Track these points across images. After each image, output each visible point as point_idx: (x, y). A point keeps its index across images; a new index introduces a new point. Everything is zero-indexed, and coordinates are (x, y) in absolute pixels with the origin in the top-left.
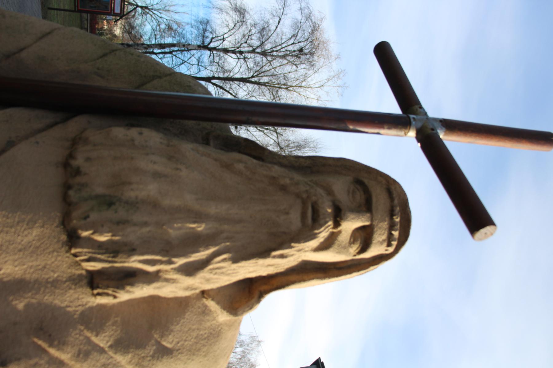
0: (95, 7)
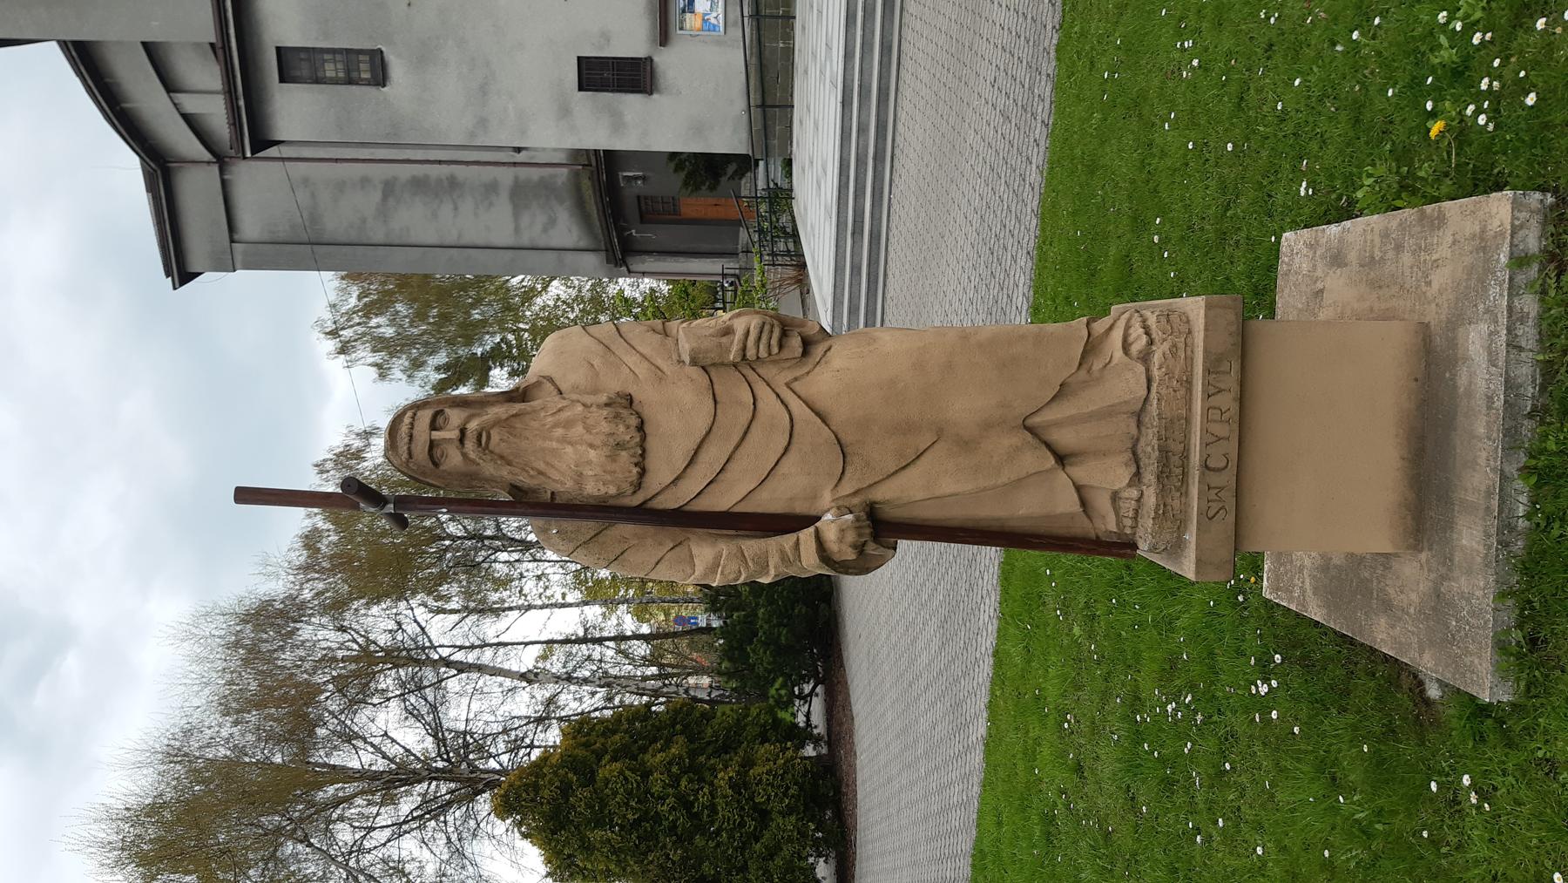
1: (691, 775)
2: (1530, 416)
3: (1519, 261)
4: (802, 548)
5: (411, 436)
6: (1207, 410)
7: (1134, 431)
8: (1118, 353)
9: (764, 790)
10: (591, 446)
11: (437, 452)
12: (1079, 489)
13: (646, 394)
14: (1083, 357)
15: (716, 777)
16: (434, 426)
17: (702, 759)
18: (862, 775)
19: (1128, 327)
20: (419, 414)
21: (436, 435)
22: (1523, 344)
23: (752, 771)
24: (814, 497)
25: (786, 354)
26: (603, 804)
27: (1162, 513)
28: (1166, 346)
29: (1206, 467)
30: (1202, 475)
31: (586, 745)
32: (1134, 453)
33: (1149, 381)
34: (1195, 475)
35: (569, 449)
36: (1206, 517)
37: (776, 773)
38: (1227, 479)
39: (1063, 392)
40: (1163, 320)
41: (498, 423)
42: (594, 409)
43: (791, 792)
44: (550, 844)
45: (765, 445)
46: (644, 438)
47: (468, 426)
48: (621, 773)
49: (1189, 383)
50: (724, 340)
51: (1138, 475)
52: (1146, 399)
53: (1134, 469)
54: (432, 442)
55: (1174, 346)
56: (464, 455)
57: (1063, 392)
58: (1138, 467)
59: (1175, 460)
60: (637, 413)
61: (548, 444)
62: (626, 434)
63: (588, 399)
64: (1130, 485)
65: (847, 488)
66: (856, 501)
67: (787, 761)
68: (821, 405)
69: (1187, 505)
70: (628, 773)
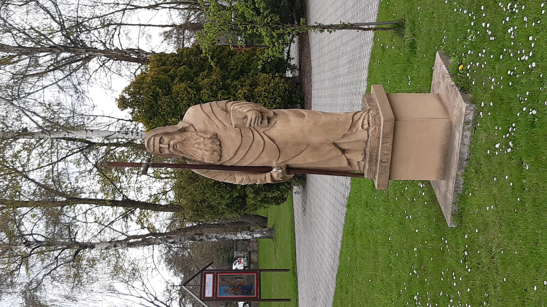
0: (236, 278)
1: (224, 91)
2: (466, 161)
3: (466, 123)
4: (267, 178)
5: (154, 146)
6: (382, 147)
7: (365, 147)
8: (360, 128)
9: (263, 100)
10: (206, 150)
11: (162, 150)
12: (348, 160)
13: (222, 134)
14: (350, 128)
15: (237, 92)
16: (160, 143)
17: (229, 81)
18: (314, 92)
19: (364, 119)
20: (155, 138)
21: (161, 145)
22: (466, 143)
23: (256, 90)
24: (271, 162)
25: (262, 124)
26: (176, 105)
27: (370, 170)
28: (373, 128)
29: (382, 162)
30: (380, 163)
31: (166, 71)
32: (365, 151)
33: (368, 136)
34: (379, 163)
35: (200, 151)
36: (381, 174)
37: (269, 91)
38: (388, 164)
39: (344, 136)
40: (373, 120)
41: (179, 142)
42: (206, 139)
43: (277, 101)
44: (149, 124)
45: (257, 149)
46: (221, 148)
47: (170, 143)
48: (186, 89)
49: (379, 138)
50: (244, 121)
51: (365, 157)
52: (368, 140)
53: (364, 156)
54: (160, 147)
55: (375, 128)
56: (169, 151)
57: (344, 136)
58: (365, 155)
59: (374, 157)
60: (219, 140)
61: (193, 149)
62: (216, 147)
63: (205, 136)
64: (362, 161)
65: (280, 161)
66: (283, 164)
67: (275, 85)
68: (273, 138)
69: (377, 169)
70: (189, 89)
